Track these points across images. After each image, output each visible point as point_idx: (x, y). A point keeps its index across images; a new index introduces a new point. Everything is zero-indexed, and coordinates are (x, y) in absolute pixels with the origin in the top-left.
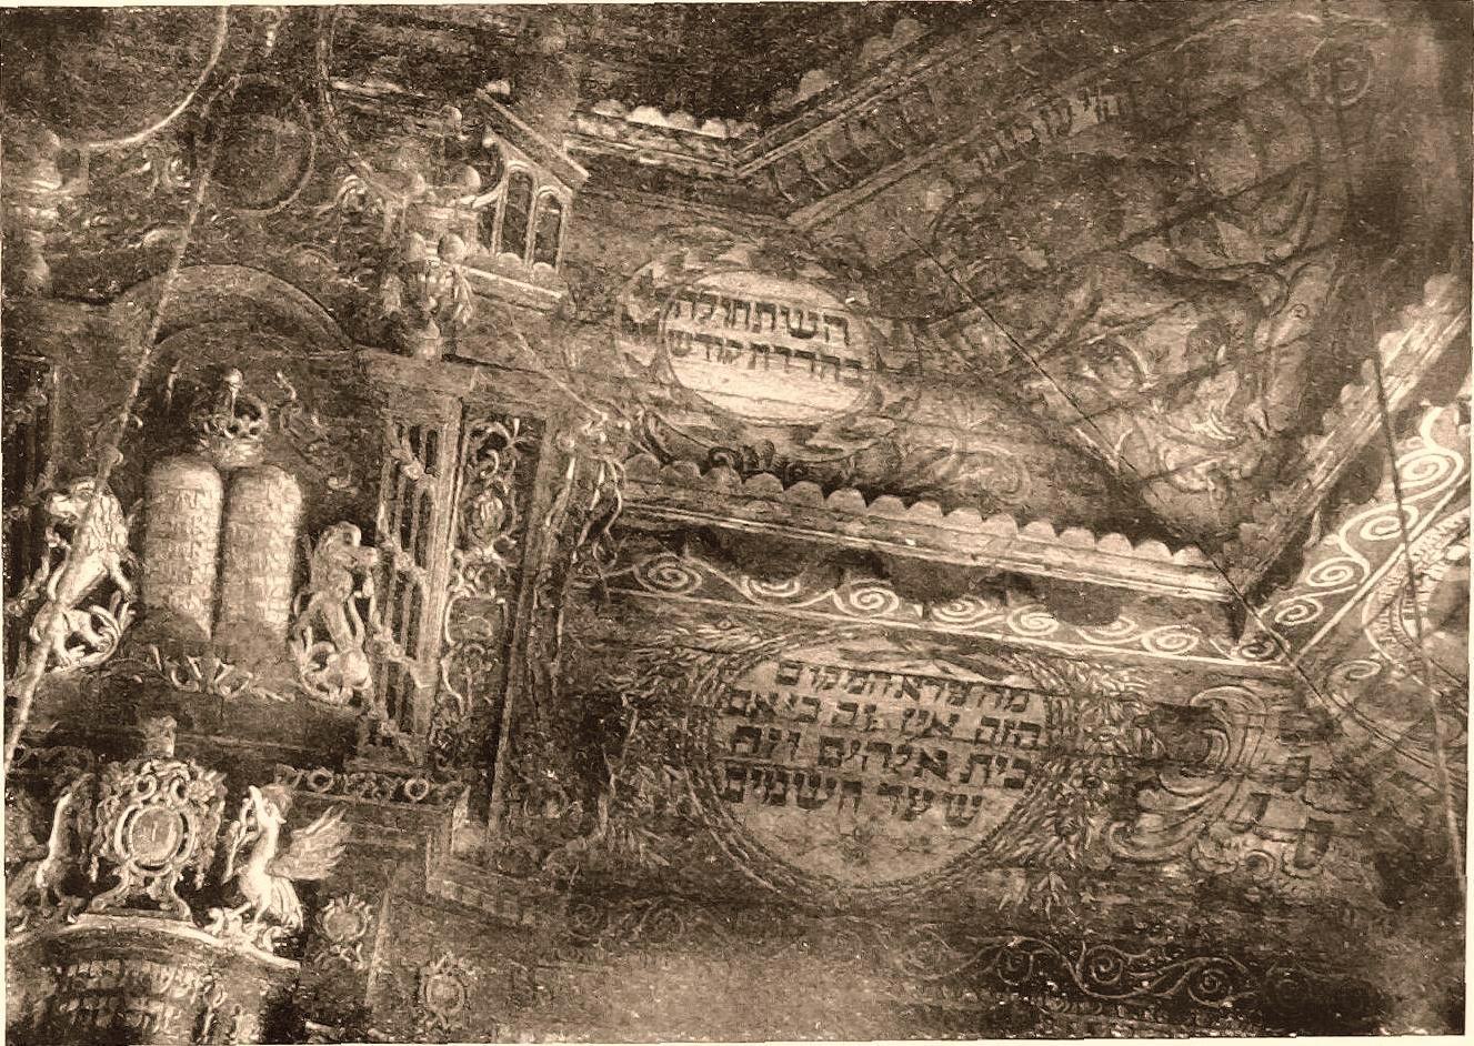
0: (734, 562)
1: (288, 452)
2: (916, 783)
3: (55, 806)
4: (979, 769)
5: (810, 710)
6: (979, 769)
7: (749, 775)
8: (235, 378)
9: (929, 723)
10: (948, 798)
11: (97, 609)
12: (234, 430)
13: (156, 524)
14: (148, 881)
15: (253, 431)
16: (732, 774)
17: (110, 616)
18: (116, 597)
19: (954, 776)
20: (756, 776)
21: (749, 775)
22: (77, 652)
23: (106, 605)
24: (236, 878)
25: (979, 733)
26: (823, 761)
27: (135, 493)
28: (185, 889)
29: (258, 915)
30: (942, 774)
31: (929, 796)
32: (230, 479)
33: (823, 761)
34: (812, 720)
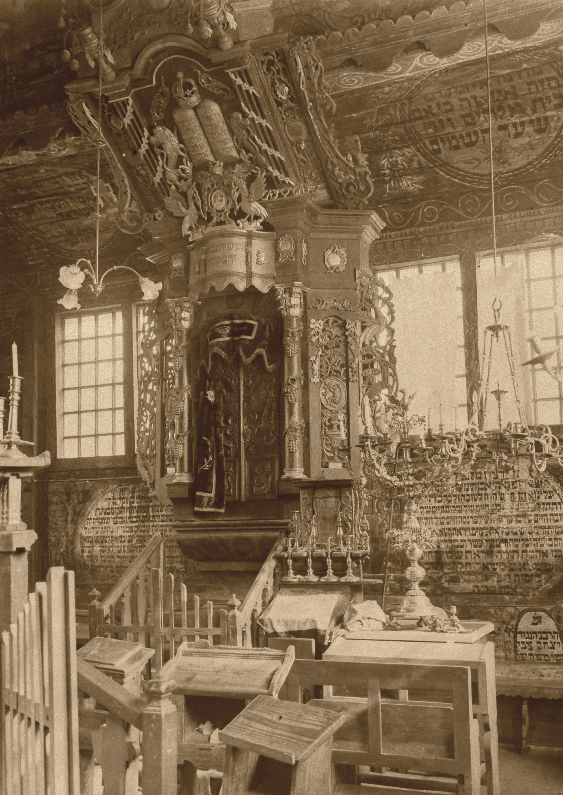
0: (499, 32)
1: (205, 94)
2: (513, 120)
3: (255, 350)
4: (539, 105)
5: (448, 107)
6: (539, 105)
7: (439, 140)
8: (180, 75)
9: (503, 94)
10: (531, 122)
11: (181, 166)
12: (186, 96)
13: (182, 129)
14: (221, 216)
15: (193, 93)
16: (432, 143)
17: (185, 167)
18: (184, 160)
19: (529, 111)
20: (443, 141)
21: (439, 140)
22: (182, 182)
23: (183, 164)
24: (240, 208)
25: (529, 89)
26: (468, 124)
27: (170, 123)
28: (232, 216)
29: (252, 218)
30: (524, 113)
31: (522, 124)
32: (195, 109)
33: (468, 124)
34: (451, 110)
